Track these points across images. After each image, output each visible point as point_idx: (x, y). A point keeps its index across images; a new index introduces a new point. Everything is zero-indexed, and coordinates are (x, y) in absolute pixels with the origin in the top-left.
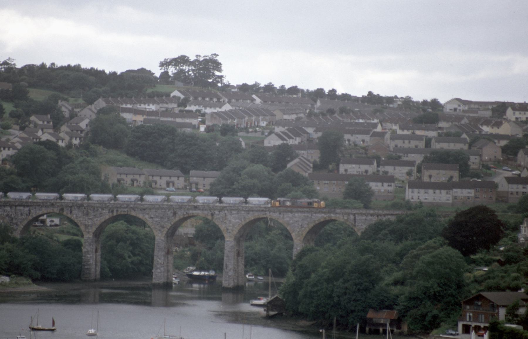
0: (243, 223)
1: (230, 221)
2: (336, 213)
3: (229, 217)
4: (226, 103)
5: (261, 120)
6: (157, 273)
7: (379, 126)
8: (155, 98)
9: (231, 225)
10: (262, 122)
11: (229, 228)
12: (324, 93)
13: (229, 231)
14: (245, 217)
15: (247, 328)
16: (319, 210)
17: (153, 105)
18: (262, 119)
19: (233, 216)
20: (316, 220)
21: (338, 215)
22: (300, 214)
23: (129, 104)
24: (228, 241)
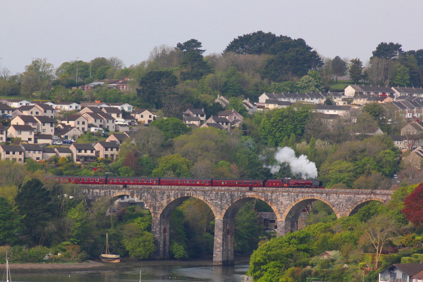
0: (294, 205)
1: (282, 202)
2: (376, 194)
3: (280, 198)
4: (387, 97)
5: (415, 111)
6: (216, 252)
7: (13, 122)
8: (398, 87)
9: (283, 206)
10: (408, 114)
11: (281, 209)
12: (250, 99)
13: (280, 212)
14: (295, 199)
15: (196, 268)
16: (306, 185)
17: (317, 99)
18: (416, 111)
19: (284, 198)
20: (358, 201)
21: (378, 196)
22: (344, 195)
23: (315, 98)
24: (280, 221)
